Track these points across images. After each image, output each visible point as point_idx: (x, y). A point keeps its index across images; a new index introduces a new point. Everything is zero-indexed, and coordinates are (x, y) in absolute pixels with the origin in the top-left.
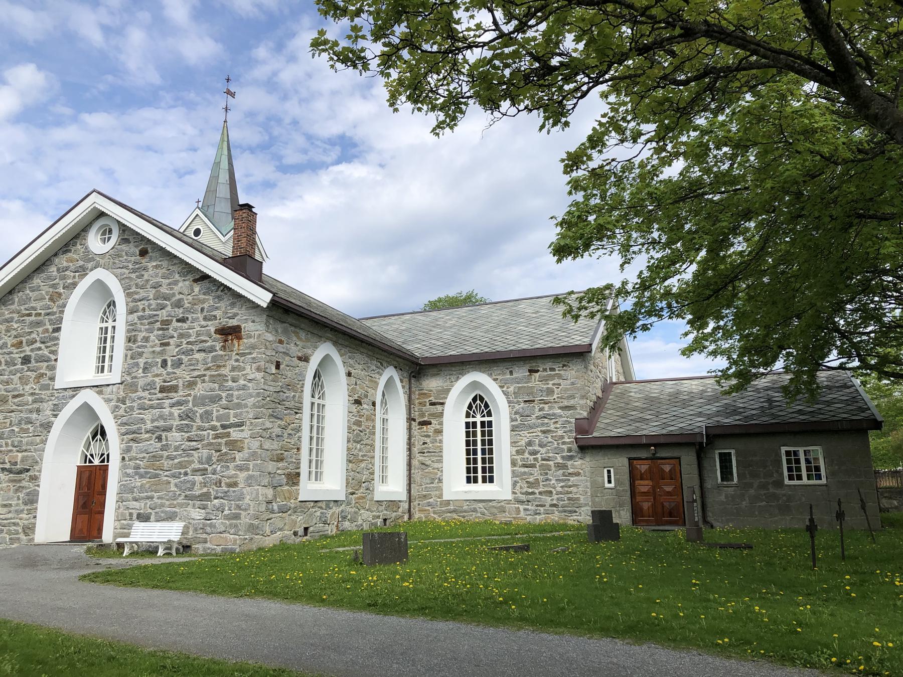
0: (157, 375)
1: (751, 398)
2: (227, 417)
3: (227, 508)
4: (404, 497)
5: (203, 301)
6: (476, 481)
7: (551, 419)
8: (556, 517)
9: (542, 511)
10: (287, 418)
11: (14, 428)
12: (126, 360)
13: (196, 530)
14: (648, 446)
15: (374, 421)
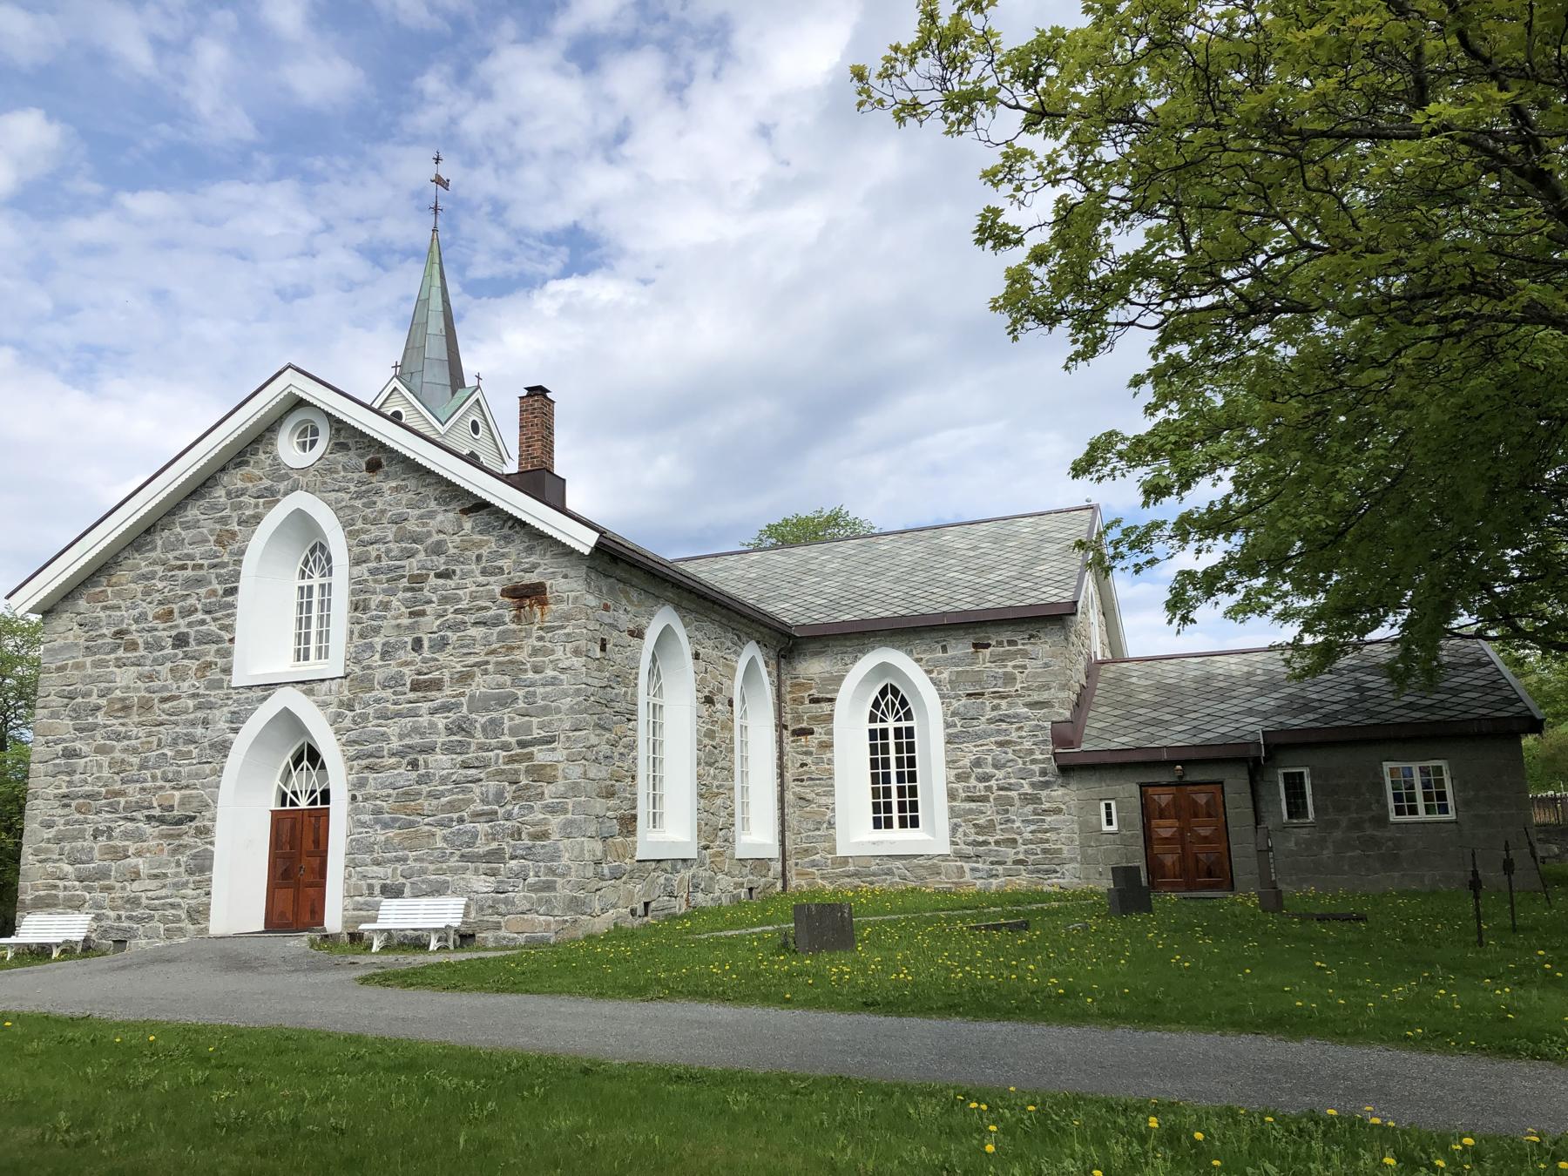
0: (406, 664)
1: (1329, 684)
2: (529, 730)
3: (531, 874)
4: (775, 853)
5: (480, 545)
6: (889, 825)
7: (1012, 723)
8: (1023, 881)
9: (1001, 872)
10: (617, 728)
11: (165, 751)
12: (351, 638)
13: (481, 909)
14: (1171, 764)
15: (731, 730)
